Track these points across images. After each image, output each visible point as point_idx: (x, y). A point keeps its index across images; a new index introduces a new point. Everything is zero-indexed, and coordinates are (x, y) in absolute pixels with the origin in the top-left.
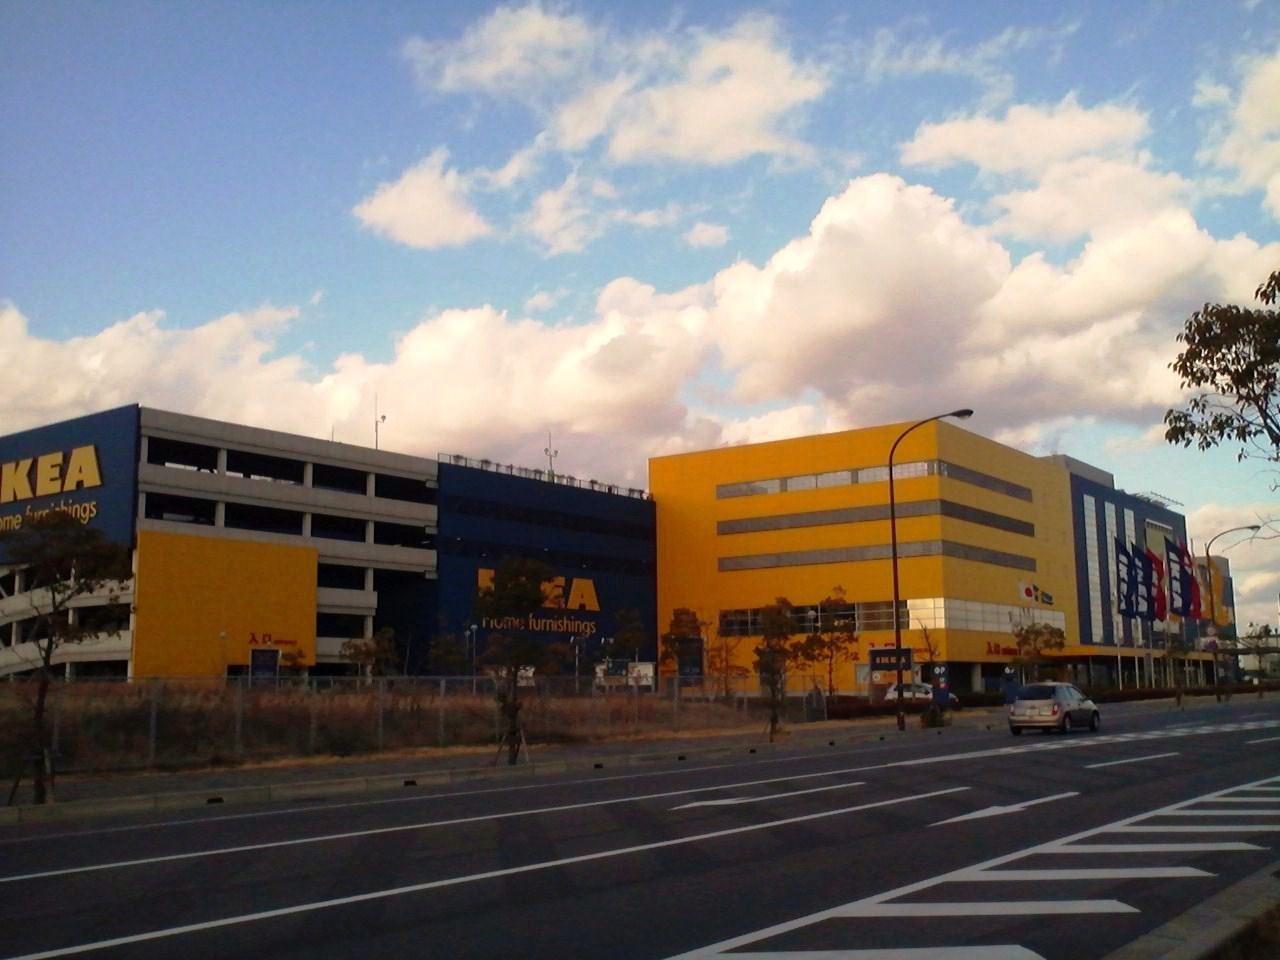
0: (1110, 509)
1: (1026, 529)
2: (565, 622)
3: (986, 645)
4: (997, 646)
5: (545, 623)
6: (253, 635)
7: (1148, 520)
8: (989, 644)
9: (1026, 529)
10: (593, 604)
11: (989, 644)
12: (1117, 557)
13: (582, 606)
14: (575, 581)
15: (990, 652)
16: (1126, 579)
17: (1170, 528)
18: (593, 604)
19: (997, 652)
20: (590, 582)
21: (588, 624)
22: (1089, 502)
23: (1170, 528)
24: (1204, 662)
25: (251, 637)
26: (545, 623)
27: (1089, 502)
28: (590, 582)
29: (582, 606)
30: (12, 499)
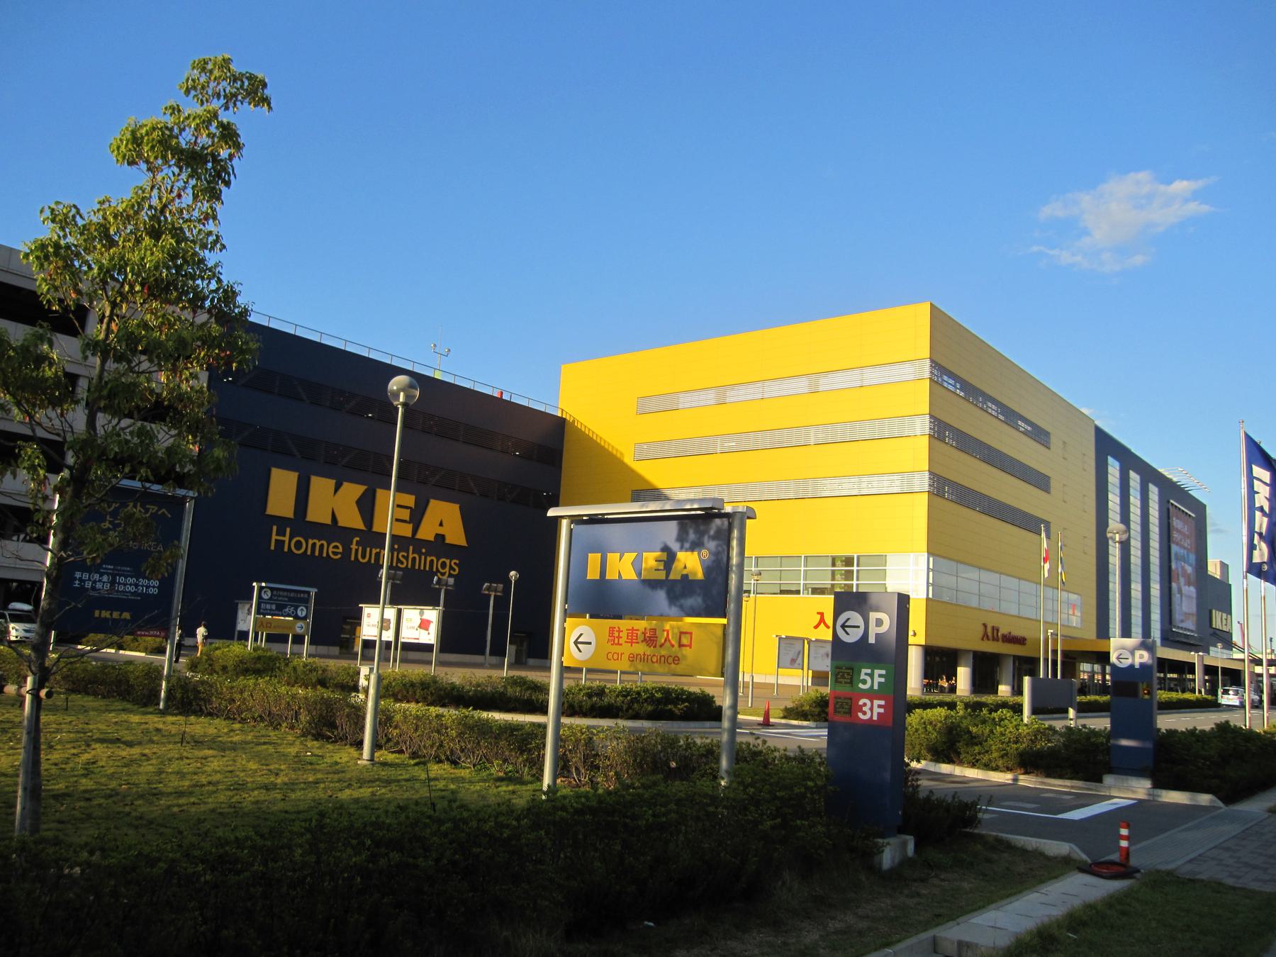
0: (1134, 478)
1: (1041, 482)
2: (411, 556)
3: (981, 629)
4: (995, 629)
5: (314, 544)
6: (822, 614)
7: (1172, 501)
8: (985, 626)
9: (1041, 482)
10: (456, 535)
11: (985, 626)
12: (1250, 471)
13: (440, 538)
14: (433, 503)
15: (985, 636)
16: (1266, 509)
17: (1193, 515)
18: (456, 535)
19: (995, 639)
20: (457, 507)
21: (448, 562)
22: (1114, 468)
23: (1193, 515)
24: (483, 653)
25: (819, 617)
26: (314, 544)
27: (1114, 468)
28: (457, 507)
29: (440, 538)
30: (346, 485)
